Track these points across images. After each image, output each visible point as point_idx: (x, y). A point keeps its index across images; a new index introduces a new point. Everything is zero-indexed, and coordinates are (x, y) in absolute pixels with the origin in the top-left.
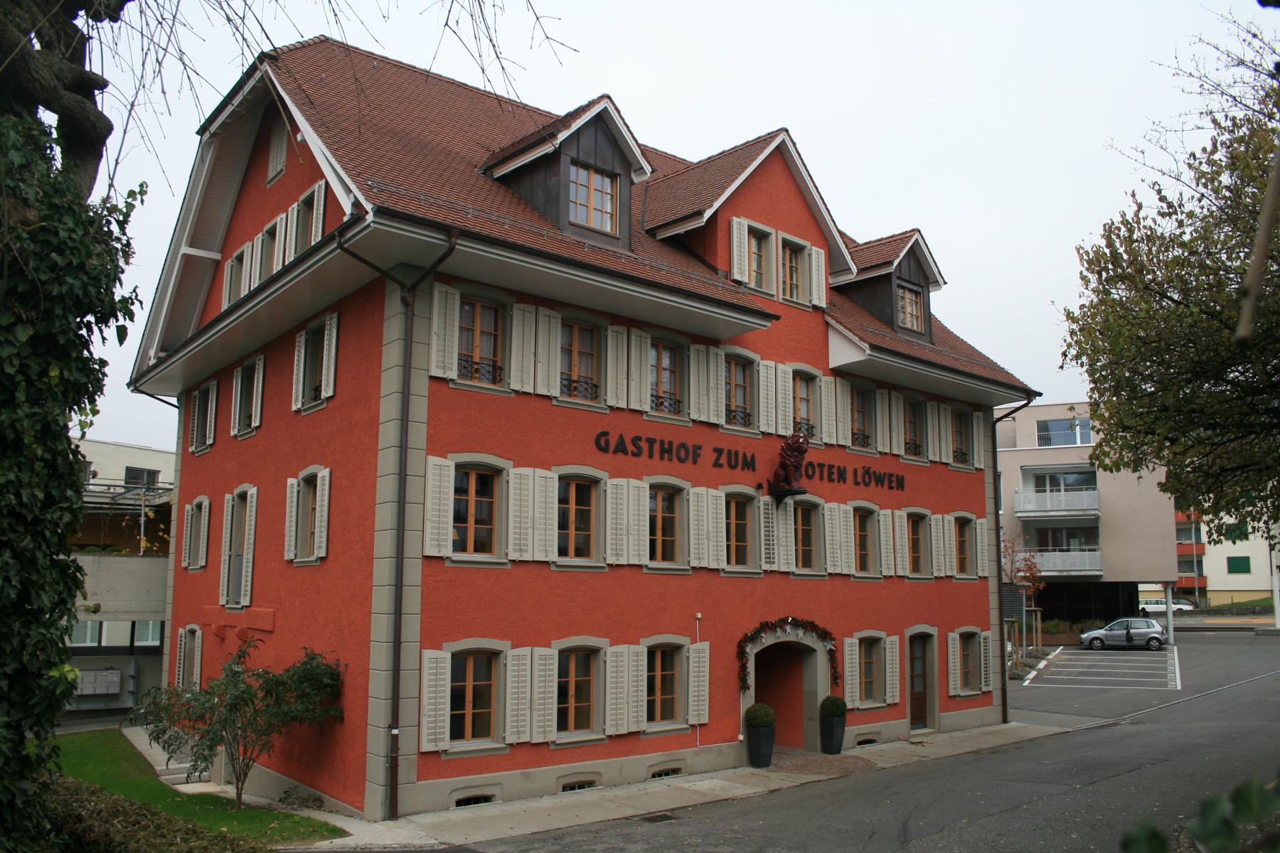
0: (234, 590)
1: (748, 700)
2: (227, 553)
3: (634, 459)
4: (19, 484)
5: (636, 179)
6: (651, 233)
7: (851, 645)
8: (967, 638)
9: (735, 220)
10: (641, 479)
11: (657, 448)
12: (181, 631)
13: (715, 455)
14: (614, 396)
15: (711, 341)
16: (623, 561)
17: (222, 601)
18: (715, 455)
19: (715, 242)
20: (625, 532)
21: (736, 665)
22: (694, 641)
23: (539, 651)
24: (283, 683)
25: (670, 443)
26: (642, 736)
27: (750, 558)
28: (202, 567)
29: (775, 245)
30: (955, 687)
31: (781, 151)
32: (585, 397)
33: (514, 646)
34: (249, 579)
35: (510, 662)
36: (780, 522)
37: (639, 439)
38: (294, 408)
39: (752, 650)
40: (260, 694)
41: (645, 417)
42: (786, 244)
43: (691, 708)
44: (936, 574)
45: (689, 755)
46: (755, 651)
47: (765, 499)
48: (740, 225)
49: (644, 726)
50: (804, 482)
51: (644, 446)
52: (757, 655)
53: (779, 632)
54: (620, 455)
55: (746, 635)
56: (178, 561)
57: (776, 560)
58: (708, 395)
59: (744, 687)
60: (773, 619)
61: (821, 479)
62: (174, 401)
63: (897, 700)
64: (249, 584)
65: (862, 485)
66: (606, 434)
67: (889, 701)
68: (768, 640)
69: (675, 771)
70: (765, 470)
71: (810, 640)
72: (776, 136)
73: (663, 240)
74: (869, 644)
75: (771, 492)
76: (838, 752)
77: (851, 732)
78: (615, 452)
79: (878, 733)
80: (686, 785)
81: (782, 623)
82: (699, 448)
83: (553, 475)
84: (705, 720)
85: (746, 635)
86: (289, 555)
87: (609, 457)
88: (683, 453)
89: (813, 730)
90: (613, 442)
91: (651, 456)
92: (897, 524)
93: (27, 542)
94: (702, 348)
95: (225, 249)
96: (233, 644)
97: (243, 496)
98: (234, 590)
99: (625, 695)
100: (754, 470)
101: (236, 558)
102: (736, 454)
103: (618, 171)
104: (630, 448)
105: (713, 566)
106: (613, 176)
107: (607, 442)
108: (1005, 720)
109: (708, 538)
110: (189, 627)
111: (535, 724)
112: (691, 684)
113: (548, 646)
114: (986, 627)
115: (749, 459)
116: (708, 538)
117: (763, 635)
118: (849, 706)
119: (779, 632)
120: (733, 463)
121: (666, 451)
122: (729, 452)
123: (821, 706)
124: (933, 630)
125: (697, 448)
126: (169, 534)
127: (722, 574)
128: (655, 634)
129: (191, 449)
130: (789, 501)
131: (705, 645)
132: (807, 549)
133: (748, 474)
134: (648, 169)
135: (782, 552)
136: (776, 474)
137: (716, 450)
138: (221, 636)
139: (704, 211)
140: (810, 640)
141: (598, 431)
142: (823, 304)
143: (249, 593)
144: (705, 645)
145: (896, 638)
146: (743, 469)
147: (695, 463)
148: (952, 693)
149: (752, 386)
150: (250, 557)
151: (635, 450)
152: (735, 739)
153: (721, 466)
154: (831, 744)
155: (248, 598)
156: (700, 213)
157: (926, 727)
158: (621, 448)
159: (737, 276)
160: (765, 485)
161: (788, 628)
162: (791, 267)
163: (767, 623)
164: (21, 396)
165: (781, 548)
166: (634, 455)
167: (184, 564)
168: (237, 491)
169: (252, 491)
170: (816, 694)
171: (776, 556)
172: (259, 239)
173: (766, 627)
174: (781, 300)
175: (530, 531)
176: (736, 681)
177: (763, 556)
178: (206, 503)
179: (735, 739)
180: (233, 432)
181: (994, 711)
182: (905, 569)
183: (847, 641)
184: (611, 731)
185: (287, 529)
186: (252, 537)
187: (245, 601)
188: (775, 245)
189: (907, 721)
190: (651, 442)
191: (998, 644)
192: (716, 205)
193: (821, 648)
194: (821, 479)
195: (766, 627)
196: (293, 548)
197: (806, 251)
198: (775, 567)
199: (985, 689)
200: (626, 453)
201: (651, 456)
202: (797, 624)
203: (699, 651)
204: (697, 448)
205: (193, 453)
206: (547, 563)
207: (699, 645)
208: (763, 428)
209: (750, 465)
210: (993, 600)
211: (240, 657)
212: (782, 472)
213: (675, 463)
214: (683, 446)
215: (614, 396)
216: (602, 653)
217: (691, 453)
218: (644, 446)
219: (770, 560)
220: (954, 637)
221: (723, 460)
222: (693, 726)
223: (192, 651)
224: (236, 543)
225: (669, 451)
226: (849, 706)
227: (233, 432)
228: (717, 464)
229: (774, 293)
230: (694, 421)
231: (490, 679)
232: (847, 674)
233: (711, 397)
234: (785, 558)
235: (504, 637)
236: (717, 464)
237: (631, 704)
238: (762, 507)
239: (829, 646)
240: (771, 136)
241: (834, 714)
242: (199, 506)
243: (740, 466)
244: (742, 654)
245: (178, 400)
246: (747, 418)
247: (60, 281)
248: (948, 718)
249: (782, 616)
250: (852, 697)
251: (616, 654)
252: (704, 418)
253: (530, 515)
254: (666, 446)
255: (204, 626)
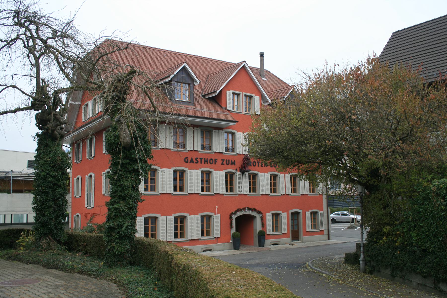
0: (89, 203)
1: (233, 230)
2: (87, 192)
3: (196, 164)
4: (61, 191)
5: (195, 84)
6: (204, 96)
7: (269, 215)
8: (314, 214)
9: (228, 92)
10: (198, 170)
11: (203, 161)
12: (74, 215)
13: (222, 161)
14: (189, 147)
15: (220, 128)
16: (193, 192)
17: (86, 206)
18: (222, 161)
19: (222, 99)
20: (193, 184)
21: (229, 221)
22: (215, 214)
23: (168, 217)
24: (102, 226)
25: (207, 159)
26: (199, 240)
27: (234, 191)
28: (80, 197)
29: (242, 97)
30: (308, 228)
31: (244, 67)
32: (182, 148)
33: (161, 216)
34: (93, 200)
35: (160, 220)
36: (244, 179)
37: (198, 158)
38: (103, 152)
39: (234, 217)
40: (96, 229)
41: (199, 152)
42: (246, 96)
43: (214, 233)
44: (301, 193)
45: (214, 246)
46: (236, 217)
47: (238, 173)
48: (229, 93)
49: (200, 237)
50: (250, 168)
51: (199, 160)
52: (236, 218)
53: (243, 211)
54: (192, 163)
55: (232, 212)
56: (73, 195)
57: (242, 191)
58: (219, 144)
59: (232, 227)
60: (241, 208)
61: (258, 166)
62: (68, 146)
63: (286, 232)
64: (93, 201)
65: (273, 167)
66: (187, 158)
67: (283, 232)
68: (239, 214)
69: (210, 250)
70: (239, 164)
71: (254, 214)
72: (242, 64)
73: (207, 98)
74: (276, 216)
75: (240, 171)
76: (263, 246)
77: (268, 242)
78: (190, 163)
79: (279, 242)
80: (213, 253)
81: (245, 209)
82: (217, 160)
83: (172, 171)
84: (219, 236)
85: (232, 212)
86: (103, 193)
87: (188, 164)
88: (211, 162)
89: (256, 240)
90: (189, 160)
91: (201, 163)
92: (286, 178)
93: (63, 198)
94: (217, 131)
95: (81, 101)
96: (89, 217)
97: (91, 176)
98: (89, 203)
99: (194, 229)
100: (235, 165)
101: (89, 194)
102: (229, 160)
103: (189, 83)
104: (195, 161)
105: (221, 193)
106: (189, 84)
107: (188, 160)
108: (329, 239)
109: (220, 185)
110: (77, 214)
111: (168, 236)
112: (214, 226)
113: (171, 215)
114: (322, 209)
115: (233, 162)
116: (220, 185)
117: (238, 212)
118: (268, 233)
119: (243, 211)
120: (228, 163)
121: (206, 161)
122: (227, 160)
123: (259, 232)
124: (300, 211)
125: (216, 160)
126: (69, 187)
127: (224, 195)
128: (203, 212)
129: (75, 161)
130: (247, 173)
131: (219, 215)
132: (253, 186)
133: (233, 166)
134: (198, 81)
135: (244, 188)
136: (242, 166)
137: (222, 160)
138: (86, 216)
139: (217, 91)
140: (254, 214)
141: (185, 157)
142: (259, 113)
143: (93, 204)
144: (219, 215)
145: (286, 213)
146: (231, 165)
147: (215, 164)
148: (307, 230)
149: (234, 140)
150: (93, 193)
151: (196, 162)
152: (229, 242)
153: (224, 164)
154: (261, 244)
155: (93, 205)
156: (215, 92)
157: (299, 241)
158: (192, 161)
159: (228, 109)
160: (238, 169)
161: (246, 210)
162: (249, 103)
163: (239, 209)
164: (61, 180)
165: (244, 187)
166: (196, 163)
167: (75, 196)
168: (89, 174)
169: (93, 175)
170: (257, 229)
171: (242, 189)
172: (92, 101)
173: (239, 210)
174: (244, 114)
175: (165, 185)
176: (229, 225)
177: (238, 189)
178: (80, 178)
179: (229, 242)
180: (87, 157)
181: (325, 236)
182: (289, 192)
183: (267, 214)
184: (190, 238)
185: (103, 186)
186: (94, 188)
187: (92, 206)
188: (242, 97)
189: (290, 239)
190: (201, 159)
191: (326, 215)
192: (221, 89)
193: (258, 217)
194: (258, 166)
195: (239, 210)
196: (104, 191)
197: (253, 97)
198: (242, 193)
199: (321, 229)
200: (193, 162)
201: (201, 163)
202: (249, 209)
203: (217, 217)
204: (216, 160)
205: (76, 163)
206: (170, 194)
207: (217, 215)
208: (238, 152)
209: (233, 163)
210: (325, 201)
211: (91, 220)
212: (243, 165)
213: (209, 164)
214: (212, 159)
215: (189, 147)
216: (187, 217)
217: (214, 161)
218: (199, 160)
219: (240, 190)
220: (308, 214)
221: (225, 162)
222: (215, 238)
223: (78, 221)
224: (90, 189)
225: (207, 161)
226: (268, 233)
227: (87, 157)
228: (222, 164)
229: (242, 112)
230: (215, 152)
231: (155, 224)
232: (267, 224)
233: (220, 145)
234: (245, 190)
235: (159, 213)
236: (222, 164)
237: (196, 231)
238: (237, 176)
239: (261, 215)
240: (241, 63)
241: (262, 236)
242: (78, 178)
243: (230, 164)
244: (231, 218)
245: (70, 145)
246: (233, 150)
247: (64, 166)
248: (306, 238)
249: (244, 207)
250: (269, 230)
251: (191, 218)
252: (218, 151)
253: (165, 181)
254: (206, 160)
255: (81, 213)
